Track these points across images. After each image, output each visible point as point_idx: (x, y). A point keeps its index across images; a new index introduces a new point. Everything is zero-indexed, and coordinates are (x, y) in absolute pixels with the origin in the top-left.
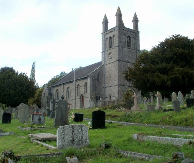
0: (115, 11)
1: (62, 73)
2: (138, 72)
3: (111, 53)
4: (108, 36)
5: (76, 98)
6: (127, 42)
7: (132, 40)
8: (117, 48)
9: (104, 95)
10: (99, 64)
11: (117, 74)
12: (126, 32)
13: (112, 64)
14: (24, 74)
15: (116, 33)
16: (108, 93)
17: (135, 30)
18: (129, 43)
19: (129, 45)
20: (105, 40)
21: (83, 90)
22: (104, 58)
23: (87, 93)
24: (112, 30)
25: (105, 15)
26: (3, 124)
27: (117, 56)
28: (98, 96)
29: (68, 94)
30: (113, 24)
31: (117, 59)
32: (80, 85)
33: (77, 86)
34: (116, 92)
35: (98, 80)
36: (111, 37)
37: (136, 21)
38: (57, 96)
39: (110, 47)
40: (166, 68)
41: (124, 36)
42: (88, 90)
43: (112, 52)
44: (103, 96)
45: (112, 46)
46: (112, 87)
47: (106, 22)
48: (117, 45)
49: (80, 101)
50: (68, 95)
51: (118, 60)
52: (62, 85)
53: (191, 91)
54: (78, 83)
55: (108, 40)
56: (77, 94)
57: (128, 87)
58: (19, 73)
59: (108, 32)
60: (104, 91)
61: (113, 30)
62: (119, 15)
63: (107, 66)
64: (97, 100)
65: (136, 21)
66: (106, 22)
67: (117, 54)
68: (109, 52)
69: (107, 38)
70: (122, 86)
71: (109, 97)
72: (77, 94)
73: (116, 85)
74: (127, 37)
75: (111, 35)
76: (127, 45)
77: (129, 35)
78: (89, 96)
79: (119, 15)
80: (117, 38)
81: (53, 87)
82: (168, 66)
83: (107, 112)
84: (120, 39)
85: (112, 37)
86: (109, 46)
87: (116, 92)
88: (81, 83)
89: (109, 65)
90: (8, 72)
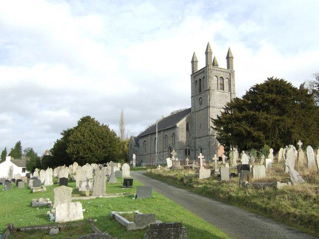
1: (86, 121)
2: (223, 121)
4: (198, 78)
6: (219, 84)
7: (226, 81)
9: (195, 147)
10: (188, 111)
11: (76, 220)
12: (218, 72)
18: (223, 85)
19: (223, 89)
21: (171, 142)
22: (193, 104)
28: (188, 148)
32: (168, 136)
33: (164, 137)
36: (200, 80)
37: (229, 58)
41: (215, 78)
44: (193, 148)
54: (166, 133)
60: (195, 143)
64: (186, 154)
65: (229, 58)
66: (194, 62)
69: (196, 81)
71: (200, 150)
74: (219, 78)
75: (201, 76)
76: (219, 88)
77: (222, 76)
79: (208, 53)
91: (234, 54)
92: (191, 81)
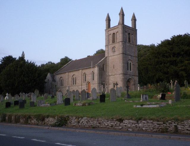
0: (119, 11)
3: (114, 47)
4: (112, 32)
5: (83, 84)
8: (121, 43)
13: (116, 56)
14: (33, 63)
15: (120, 30)
16: (112, 80)
17: (133, 27)
20: (108, 36)
22: (139, 46)
23: (93, 80)
24: (115, 27)
25: (108, 14)
26: (16, 106)
27: (121, 50)
29: (73, 81)
30: (115, 22)
31: (121, 52)
33: (83, 74)
34: (120, 79)
35: (103, 70)
37: (134, 20)
38: (60, 83)
39: (114, 41)
40: (175, 61)
42: (95, 77)
43: (116, 46)
45: (115, 41)
46: (116, 76)
47: (108, 20)
48: (121, 41)
49: (86, 87)
50: (74, 82)
51: (122, 54)
52: (67, 73)
53: (184, 82)
55: (111, 36)
56: (83, 81)
57: (129, 76)
58: (29, 62)
59: (110, 29)
60: (108, 79)
61: (115, 28)
62: (122, 14)
63: (110, 58)
65: (134, 20)
66: (108, 20)
67: (121, 48)
68: (113, 46)
70: (125, 75)
72: (83, 81)
73: (120, 74)
75: (115, 31)
78: (97, 82)
79: (122, 14)
80: (121, 34)
81: (56, 74)
82: (177, 59)
83: (99, 102)
84: (123, 35)
85: (115, 34)
86: (113, 41)
87: (120, 79)
88: (88, 72)
89: (113, 57)
90: (9, 60)
91: (111, 19)
92: (106, 34)
